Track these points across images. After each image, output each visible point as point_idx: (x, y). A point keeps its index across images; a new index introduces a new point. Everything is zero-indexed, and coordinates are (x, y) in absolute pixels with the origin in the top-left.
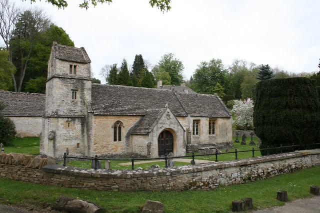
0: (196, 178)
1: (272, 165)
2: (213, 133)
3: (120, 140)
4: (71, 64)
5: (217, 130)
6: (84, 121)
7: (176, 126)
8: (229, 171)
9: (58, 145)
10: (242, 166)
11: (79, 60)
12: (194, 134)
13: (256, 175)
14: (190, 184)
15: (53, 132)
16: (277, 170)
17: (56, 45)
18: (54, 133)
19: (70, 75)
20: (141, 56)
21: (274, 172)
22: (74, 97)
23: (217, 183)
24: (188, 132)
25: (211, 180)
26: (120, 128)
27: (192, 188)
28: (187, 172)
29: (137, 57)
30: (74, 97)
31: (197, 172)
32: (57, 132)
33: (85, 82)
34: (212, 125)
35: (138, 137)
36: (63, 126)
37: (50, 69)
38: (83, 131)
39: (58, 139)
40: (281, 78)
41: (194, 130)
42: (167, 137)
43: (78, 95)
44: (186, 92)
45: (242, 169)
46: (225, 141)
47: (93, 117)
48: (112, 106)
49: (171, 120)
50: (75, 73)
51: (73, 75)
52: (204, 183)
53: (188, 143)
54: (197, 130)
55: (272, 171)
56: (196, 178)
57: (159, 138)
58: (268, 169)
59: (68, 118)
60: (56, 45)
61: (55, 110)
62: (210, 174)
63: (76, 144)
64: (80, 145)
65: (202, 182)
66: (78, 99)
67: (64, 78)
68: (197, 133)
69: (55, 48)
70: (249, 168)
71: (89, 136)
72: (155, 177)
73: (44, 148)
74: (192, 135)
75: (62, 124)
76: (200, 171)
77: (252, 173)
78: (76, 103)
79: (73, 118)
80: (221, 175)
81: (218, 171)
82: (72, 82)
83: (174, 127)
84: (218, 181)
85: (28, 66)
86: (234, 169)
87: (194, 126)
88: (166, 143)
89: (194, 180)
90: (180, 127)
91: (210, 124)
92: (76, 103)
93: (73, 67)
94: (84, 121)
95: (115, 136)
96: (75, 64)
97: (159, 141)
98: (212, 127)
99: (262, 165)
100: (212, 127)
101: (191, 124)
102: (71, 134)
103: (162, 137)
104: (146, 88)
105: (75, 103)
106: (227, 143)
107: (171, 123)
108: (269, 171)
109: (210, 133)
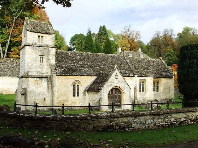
0: (113, 123)
1: (185, 116)
2: (158, 91)
3: (78, 95)
4: (39, 34)
5: (161, 88)
6: (50, 79)
7: (123, 84)
8: (143, 119)
9: (29, 99)
10: (155, 115)
11: (45, 32)
12: (140, 91)
13: (169, 123)
14: (108, 127)
15: (24, 89)
16: (189, 120)
17: (27, 20)
18: (25, 89)
19: (38, 44)
20: (104, 27)
21: (187, 121)
22: (42, 61)
23: (132, 127)
24: (135, 89)
25: (126, 125)
26: (78, 86)
27: (109, 130)
28: (105, 117)
29: (101, 28)
30: (42, 61)
31: (114, 118)
32: (28, 89)
33: (50, 49)
34: (156, 84)
36: (32, 84)
37: (23, 40)
38: (48, 88)
39: (29, 94)
40: (186, 45)
41: (140, 88)
42: (115, 94)
43: (45, 60)
44: (142, 56)
45: (155, 117)
46: (168, 98)
47: (57, 77)
48: (72, 68)
49: (119, 79)
50: (42, 42)
51: (41, 44)
52: (120, 127)
53: (135, 99)
54: (143, 88)
55: (185, 121)
56: (113, 123)
57: (109, 94)
58: (181, 119)
59: (37, 78)
60: (27, 20)
61: (26, 72)
62: (126, 120)
63: (43, 99)
64: (46, 100)
65: (118, 126)
66: (45, 63)
67: (34, 46)
68: (143, 91)
69: (27, 22)
70: (163, 117)
71: (52, 92)
72: (79, 120)
74: (138, 92)
75: (32, 83)
76: (117, 117)
77: (166, 121)
78: (43, 66)
79: (41, 78)
80: (136, 121)
81: (133, 118)
82: (40, 49)
83: (122, 85)
84: (133, 126)
85: (12, 37)
86: (148, 117)
87: (140, 85)
88: (114, 98)
89: (111, 124)
90: (126, 85)
91: (154, 83)
92: (43, 66)
93: (41, 37)
94: (50, 79)
95: (74, 93)
96: (42, 35)
97: (109, 96)
98: (156, 85)
99: (174, 115)
100: (156, 85)
101: (138, 83)
102: (39, 90)
103: (112, 93)
104: (101, 54)
105: (42, 66)
106: (170, 99)
107: (119, 82)
108: (182, 120)
109: (154, 90)
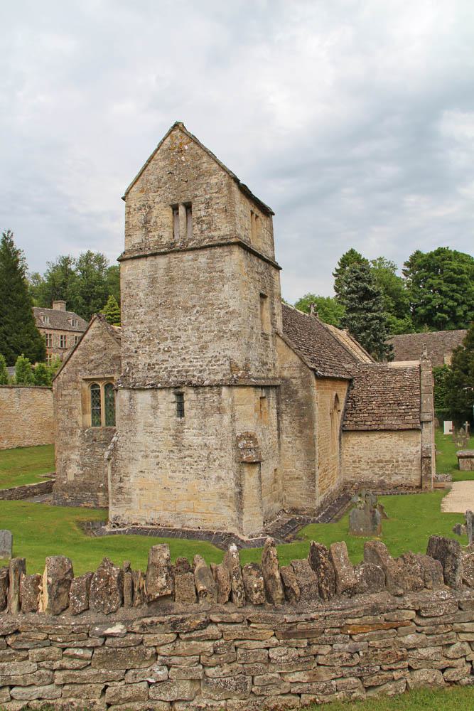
35: (374, 437)
73: (130, 500)
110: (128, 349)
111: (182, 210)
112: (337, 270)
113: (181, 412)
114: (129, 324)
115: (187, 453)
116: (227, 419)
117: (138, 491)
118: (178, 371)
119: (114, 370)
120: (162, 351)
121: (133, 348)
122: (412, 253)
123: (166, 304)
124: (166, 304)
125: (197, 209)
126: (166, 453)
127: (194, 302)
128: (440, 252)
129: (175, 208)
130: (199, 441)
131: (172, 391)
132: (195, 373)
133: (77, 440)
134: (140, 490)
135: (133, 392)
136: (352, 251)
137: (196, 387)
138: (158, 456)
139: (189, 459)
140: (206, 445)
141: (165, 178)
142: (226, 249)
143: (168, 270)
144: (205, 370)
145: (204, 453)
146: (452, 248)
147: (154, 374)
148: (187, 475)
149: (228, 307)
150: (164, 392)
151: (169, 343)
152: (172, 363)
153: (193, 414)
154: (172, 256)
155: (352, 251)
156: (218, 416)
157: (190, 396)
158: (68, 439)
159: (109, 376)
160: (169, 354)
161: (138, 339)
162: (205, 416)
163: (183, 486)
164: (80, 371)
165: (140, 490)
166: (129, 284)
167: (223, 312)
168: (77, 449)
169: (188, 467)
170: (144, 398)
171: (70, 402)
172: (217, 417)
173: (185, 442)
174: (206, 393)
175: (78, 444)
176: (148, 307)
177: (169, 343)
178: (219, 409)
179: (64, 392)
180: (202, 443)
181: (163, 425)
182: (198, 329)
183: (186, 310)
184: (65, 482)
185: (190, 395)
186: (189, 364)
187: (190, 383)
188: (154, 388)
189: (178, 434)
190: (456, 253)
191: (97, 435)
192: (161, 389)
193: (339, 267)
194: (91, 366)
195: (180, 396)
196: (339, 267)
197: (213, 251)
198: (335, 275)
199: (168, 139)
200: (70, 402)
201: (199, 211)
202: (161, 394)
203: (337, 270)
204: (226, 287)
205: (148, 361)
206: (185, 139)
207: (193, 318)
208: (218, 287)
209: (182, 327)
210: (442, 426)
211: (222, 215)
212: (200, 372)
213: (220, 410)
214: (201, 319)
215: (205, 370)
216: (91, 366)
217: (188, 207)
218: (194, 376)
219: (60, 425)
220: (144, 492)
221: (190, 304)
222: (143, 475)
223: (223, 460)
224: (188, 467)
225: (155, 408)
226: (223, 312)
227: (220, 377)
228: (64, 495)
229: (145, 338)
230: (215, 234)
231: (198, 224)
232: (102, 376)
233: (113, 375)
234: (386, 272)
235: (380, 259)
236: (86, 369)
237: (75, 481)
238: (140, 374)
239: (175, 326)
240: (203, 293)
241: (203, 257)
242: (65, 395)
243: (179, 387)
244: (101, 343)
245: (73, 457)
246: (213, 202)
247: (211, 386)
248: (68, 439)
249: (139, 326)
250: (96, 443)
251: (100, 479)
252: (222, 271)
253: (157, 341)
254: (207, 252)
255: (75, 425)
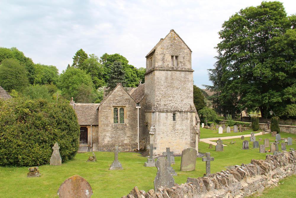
110: (157, 99)
111: (174, 58)
112: (74, 57)
113: (174, 119)
114: (158, 91)
115: (177, 131)
116: (189, 121)
117: (160, 144)
118: (174, 107)
119: (126, 104)
120: (169, 100)
121: (159, 99)
122: (104, 54)
123: (170, 86)
124: (170, 86)
125: (180, 58)
126: (170, 132)
127: (180, 87)
128: (116, 55)
129: (172, 57)
130: (180, 128)
131: (172, 113)
132: (179, 108)
133: (109, 128)
134: (161, 143)
135: (159, 113)
136: (81, 50)
137: (180, 112)
138: (167, 133)
139: (177, 133)
140: (182, 129)
141: (170, 46)
142: (190, 72)
143: (172, 76)
144: (183, 107)
145: (182, 131)
146: (120, 55)
147: (167, 107)
148: (176, 138)
149: (190, 89)
150: (170, 113)
151: (171, 98)
152: (172, 104)
153: (179, 120)
154: (173, 72)
155: (81, 50)
156: (186, 120)
157: (178, 115)
158: (105, 128)
159: (124, 105)
160: (171, 101)
161: (161, 96)
162: (183, 120)
163: (175, 141)
164: (111, 103)
165: (161, 143)
166: (158, 78)
167: (188, 91)
168: (109, 132)
169: (177, 136)
170: (163, 115)
171: (107, 114)
172: (186, 121)
173: (176, 128)
174: (183, 114)
175: (110, 130)
176: (165, 86)
177: (171, 98)
178: (187, 118)
179: (104, 111)
180: (181, 128)
181: (169, 123)
182: (181, 95)
183: (177, 89)
184: (103, 144)
185: (178, 115)
186: (177, 105)
187: (178, 111)
188: (167, 112)
189: (174, 126)
190: (122, 56)
191: (118, 127)
192: (169, 112)
193: (75, 56)
194: (117, 101)
195: (174, 114)
196: (75, 56)
197: (186, 72)
198: (74, 59)
199: (170, 34)
200: (107, 114)
201: (180, 59)
202: (169, 114)
203: (74, 57)
204: (189, 84)
205: (164, 103)
206: (176, 36)
207: (179, 92)
208: (187, 83)
209: (176, 94)
210: (201, 124)
211: (188, 62)
212: (181, 107)
213: (187, 119)
214: (182, 92)
215: (183, 107)
216: (117, 101)
217: (177, 57)
218: (179, 109)
219: (102, 122)
220: (162, 144)
221: (178, 87)
222: (162, 139)
223: (187, 133)
224: (177, 136)
225: (167, 118)
226: (188, 91)
227: (187, 109)
228: (103, 149)
229: (163, 96)
230: (186, 67)
231: (181, 63)
232: (121, 105)
233: (126, 105)
234: (93, 60)
235: (93, 54)
236: (114, 102)
237: (108, 143)
238: (162, 107)
239: (173, 93)
240: (182, 84)
241: (183, 74)
242: (105, 112)
243: (175, 112)
244: (121, 94)
245: (107, 134)
246: (185, 58)
247: (185, 112)
248: (105, 128)
249: (161, 92)
250: (118, 129)
251: (119, 142)
252: (188, 79)
253: (167, 97)
254: (184, 72)
255: (109, 123)
